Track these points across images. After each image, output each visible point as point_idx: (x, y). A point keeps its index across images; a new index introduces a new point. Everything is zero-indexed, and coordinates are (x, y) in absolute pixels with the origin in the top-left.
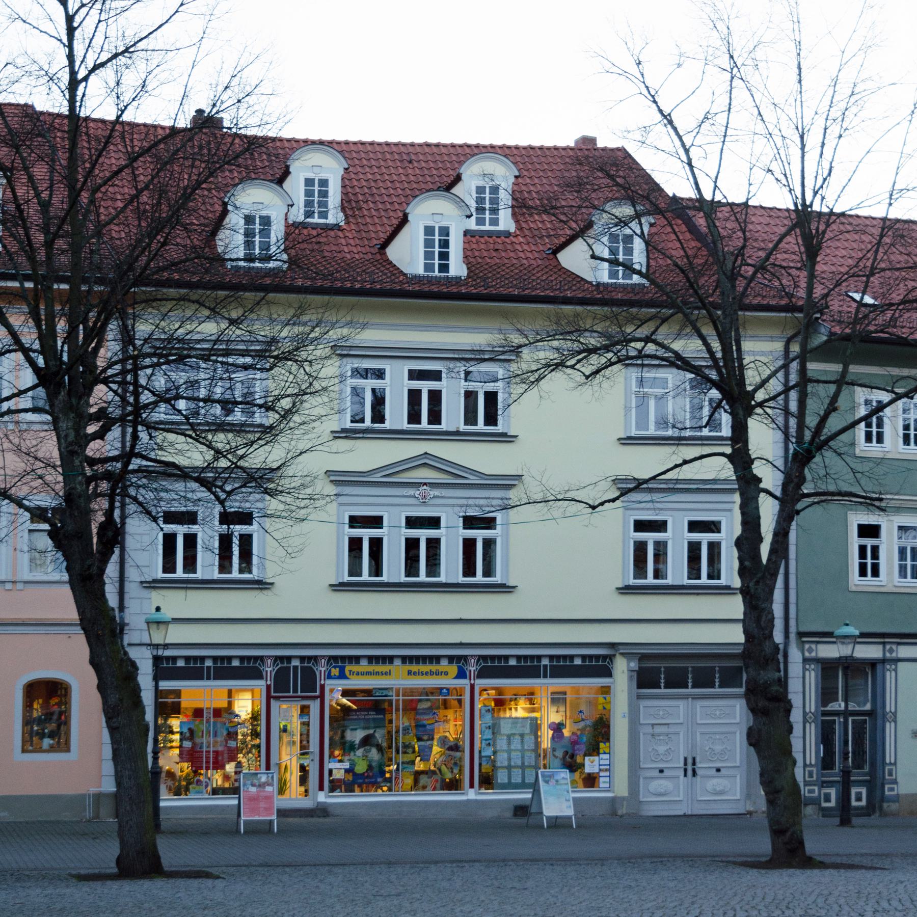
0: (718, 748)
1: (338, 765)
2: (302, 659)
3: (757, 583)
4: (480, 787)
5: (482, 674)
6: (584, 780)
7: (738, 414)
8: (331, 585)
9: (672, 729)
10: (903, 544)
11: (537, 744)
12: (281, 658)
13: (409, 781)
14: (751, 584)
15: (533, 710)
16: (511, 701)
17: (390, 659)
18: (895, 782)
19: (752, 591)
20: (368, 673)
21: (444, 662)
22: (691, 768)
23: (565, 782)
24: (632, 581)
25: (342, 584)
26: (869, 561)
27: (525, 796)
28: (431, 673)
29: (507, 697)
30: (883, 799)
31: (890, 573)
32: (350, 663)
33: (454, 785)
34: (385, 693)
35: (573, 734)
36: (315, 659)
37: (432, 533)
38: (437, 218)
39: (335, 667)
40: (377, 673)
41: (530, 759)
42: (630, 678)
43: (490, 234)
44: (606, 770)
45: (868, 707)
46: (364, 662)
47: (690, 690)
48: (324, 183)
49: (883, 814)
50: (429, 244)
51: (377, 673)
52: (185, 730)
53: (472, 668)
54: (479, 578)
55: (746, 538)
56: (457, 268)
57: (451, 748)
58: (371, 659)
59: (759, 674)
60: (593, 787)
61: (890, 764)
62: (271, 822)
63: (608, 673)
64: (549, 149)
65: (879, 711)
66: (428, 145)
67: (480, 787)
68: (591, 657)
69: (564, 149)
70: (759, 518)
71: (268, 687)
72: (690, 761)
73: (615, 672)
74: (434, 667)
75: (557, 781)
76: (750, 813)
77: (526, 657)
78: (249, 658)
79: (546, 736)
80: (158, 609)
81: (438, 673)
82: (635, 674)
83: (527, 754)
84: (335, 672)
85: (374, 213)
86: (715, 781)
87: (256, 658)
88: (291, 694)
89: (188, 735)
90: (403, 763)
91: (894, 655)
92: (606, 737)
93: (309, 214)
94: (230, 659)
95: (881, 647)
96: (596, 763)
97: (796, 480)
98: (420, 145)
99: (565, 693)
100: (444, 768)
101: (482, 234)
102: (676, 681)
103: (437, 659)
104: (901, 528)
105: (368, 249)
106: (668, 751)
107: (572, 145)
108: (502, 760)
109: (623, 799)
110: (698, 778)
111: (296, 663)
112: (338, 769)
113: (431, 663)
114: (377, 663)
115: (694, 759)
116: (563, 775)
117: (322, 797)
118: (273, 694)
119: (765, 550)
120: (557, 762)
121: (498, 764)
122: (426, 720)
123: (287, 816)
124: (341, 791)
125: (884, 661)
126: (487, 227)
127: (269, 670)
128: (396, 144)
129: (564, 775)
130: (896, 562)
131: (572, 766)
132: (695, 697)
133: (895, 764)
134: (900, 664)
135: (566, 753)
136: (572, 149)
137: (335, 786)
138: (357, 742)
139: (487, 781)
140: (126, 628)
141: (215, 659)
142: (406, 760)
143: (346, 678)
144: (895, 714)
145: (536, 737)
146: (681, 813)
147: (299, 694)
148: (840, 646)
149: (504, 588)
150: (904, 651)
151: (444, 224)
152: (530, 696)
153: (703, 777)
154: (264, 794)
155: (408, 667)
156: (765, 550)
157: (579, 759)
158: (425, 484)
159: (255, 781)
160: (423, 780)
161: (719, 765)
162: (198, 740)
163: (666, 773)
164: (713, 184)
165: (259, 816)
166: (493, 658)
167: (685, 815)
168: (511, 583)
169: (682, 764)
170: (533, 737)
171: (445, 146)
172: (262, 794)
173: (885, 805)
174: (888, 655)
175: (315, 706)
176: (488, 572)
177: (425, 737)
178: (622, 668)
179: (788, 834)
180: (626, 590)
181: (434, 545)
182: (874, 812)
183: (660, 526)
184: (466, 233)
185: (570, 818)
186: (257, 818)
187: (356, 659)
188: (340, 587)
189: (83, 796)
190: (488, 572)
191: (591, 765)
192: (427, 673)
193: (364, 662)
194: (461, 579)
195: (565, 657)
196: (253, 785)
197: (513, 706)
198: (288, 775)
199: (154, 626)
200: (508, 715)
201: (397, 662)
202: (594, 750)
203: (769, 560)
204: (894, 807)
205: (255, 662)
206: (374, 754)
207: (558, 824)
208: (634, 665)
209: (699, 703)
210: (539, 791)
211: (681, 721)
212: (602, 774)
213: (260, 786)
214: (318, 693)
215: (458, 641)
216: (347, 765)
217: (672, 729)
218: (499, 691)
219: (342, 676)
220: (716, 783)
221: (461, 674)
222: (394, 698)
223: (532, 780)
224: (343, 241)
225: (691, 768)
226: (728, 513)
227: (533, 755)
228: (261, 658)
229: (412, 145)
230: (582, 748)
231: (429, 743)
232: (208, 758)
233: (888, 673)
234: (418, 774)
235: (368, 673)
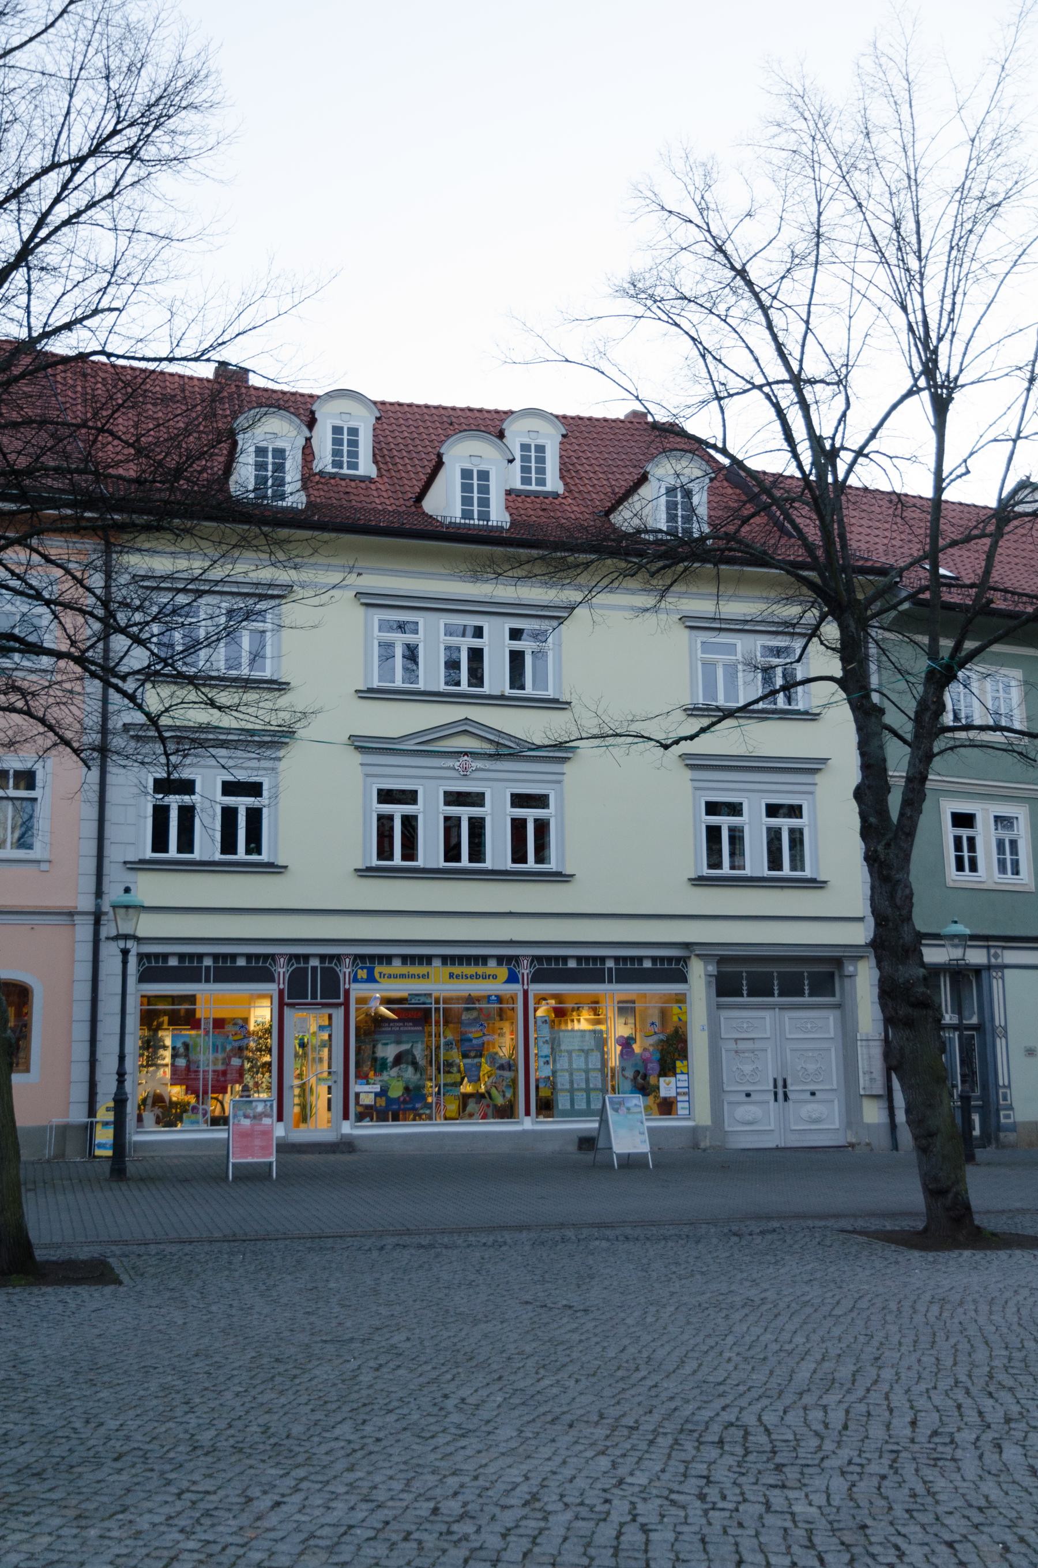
0: (811, 1067)
1: (367, 1088)
2: (322, 957)
3: (888, 845)
4: (538, 1114)
5: (537, 978)
6: (660, 1105)
7: (848, 626)
8: (356, 870)
9: (758, 1045)
10: (1001, 836)
11: (604, 1062)
12: (297, 957)
13: (453, 1107)
14: (880, 848)
15: (598, 1022)
16: (573, 1010)
17: (428, 959)
18: (1010, 1108)
19: (882, 857)
20: (402, 976)
21: (492, 963)
22: (781, 1091)
23: (637, 1110)
24: (706, 872)
25: (369, 869)
26: (966, 854)
27: (591, 1125)
28: (477, 976)
29: (569, 1006)
30: (999, 1128)
31: (989, 868)
32: (380, 963)
33: (507, 1112)
34: (422, 999)
35: (645, 1050)
36: (338, 958)
37: (475, 811)
38: (474, 460)
39: (362, 968)
40: (413, 976)
41: (596, 1081)
42: (708, 984)
43: (537, 494)
44: (684, 1094)
45: (974, 1020)
46: (397, 962)
47: (776, 999)
48: (354, 431)
49: (1001, 1146)
50: (466, 488)
51: (413, 976)
52: (179, 1045)
53: (525, 970)
54: (531, 864)
55: (869, 787)
56: (499, 515)
57: (502, 1067)
58: (405, 959)
59: (897, 970)
60: (670, 1114)
61: (1004, 1086)
62: (271, 1164)
63: (684, 979)
64: (598, 420)
65: (988, 1025)
66: (470, 410)
67: (538, 1114)
68: (662, 959)
69: (614, 421)
70: (884, 760)
71: (281, 992)
72: (780, 1083)
73: (690, 977)
74: (480, 970)
75: (628, 1109)
76: (852, 1145)
77: (587, 958)
78: (258, 957)
79: (614, 1051)
80: (127, 890)
81: (485, 977)
82: (713, 980)
83: (592, 1074)
84: (363, 974)
85: (409, 468)
86: (810, 1107)
87: (266, 957)
88: (309, 1000)
89: (182, 1050)
90: (445, 1085)
91: (999, 961)
92: (684, 1055)
93: (337, 464)
94: (234, 957)
95: (984, 951)
96: (673, 1085)
97: (933, 707)
98: (462, 410)
99: (633, 1002)
100: (494, 1091)
101: (528, 494)
102: (760, 988)
103: (484, 959)
104: (997, 818)
105: (402, 502)
106: (755, 1071)
107: (622, 417)
108: (563, 1081)
109: (705, 1128)
110: (790, 1103)
111: (314, 962)
112: (366, 1092)
113: (477, 964)
114: (413, 963)
115: (785, 1081)
116: (635, 1101)
117: (347, 1128)
118: (286, 1000)
119: (894, 802)
120: (628, 1085)
121: (559, 1086)
122: (474, 1032)
123: (304, 1152)
124: (372, 1120)
125: (989, 967)
126: (533, 487)
127: (282, 971)
128: (436, 408)
129: (637, 1101)
130: (995, 856)
131: (644, 1087)
132: (783, 1008)
133: (1009, 1087)
134: (1007, 971)
135: (637, 1072)
136: (622, 421)
137: (366, 1114)
138: (391, 1059)
139: (546, 1107)
140: (104, 918)
141: (216, 957)
142: (449, 1081)
143: (376, 981)
144: (1005, 1029)
145: (603, 1053)
146: (772, 1145)
147: (319, 1000)
148: (950, 949)
149: (560, 877)
150: (1010, 957)
151: (484, 467)
152: (595, 1006)
153: (795, 1102)
154: (261, 1128)
155: (450, 969)
156: (894, 802)
157: (652, 1080)
158: (466, 754)
159: (250, 1112)
160: (472, 1106)
161: (812, 1087)
162: (193, 1057)
163: (754, 1097)
164: (803, 326)
165: (253, 1156)
166: (549, 958)
167: (777, 1148)
168: (281, 862)
169: (771, 1087)
170: (599, 1055)
171: (488, 412)
172: (257, 1128)
173: (1002, 1135)
174: (993, 960)
175: (338, 1014)
176: (540, 858)
177: (472, 1054)
178: (698, 972)
179: (950, 1196)
180: (700, 881)
181: (477, 827)
182: (990, 1143)
183: (735, 809)
184: (509, 492)
185: (645, 1155)
186: (250, 1160)
187: (388, 959)
188: (367, 872)
189: (43, 1129)
190: (540, 858)
191: (667, 1087)
192: (471, 977)
193: (397, 962)
194: (510, 866)
195: (632, 959)
196: (246, 1116)
197: (575, 1018)
198: (313, 1099)
199: (123, 911)
200: (570, 1027)
201: (437, 963)
202: (667, 1069)
203: (902, 814)
204: (1012, 1137)
205: (265, 962)
206: (409, 1073)
207: (631, 1163)
208: (712, 969)
209: (788, 1015)
210: (607, 1121)
211: (768, 1035)
212: (680, 1098)
213: (255, 1117)
214: (342, 1000)
215: (507, 938)
216: (377, 1088)
217: (758, 1045)
218: (558, 997)
219: (371, 979)
220: (812, 1109)
221: (512, 978)
222: (433, 1006)
223: (599, 1106)
224: (375, 493)
225: (781, 1091)
226: (809, 797)
227: (599, 1075)
228: (273, 957)
229: (454, 409)
230: (654, 1067)
231: (476, 1060)
232: (205, 1080)
233: (994, 981)
234: (466, 1097)
235: (402, 976)
